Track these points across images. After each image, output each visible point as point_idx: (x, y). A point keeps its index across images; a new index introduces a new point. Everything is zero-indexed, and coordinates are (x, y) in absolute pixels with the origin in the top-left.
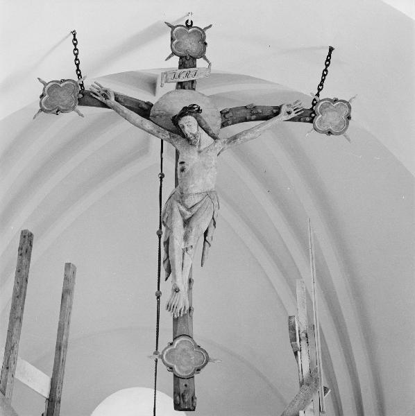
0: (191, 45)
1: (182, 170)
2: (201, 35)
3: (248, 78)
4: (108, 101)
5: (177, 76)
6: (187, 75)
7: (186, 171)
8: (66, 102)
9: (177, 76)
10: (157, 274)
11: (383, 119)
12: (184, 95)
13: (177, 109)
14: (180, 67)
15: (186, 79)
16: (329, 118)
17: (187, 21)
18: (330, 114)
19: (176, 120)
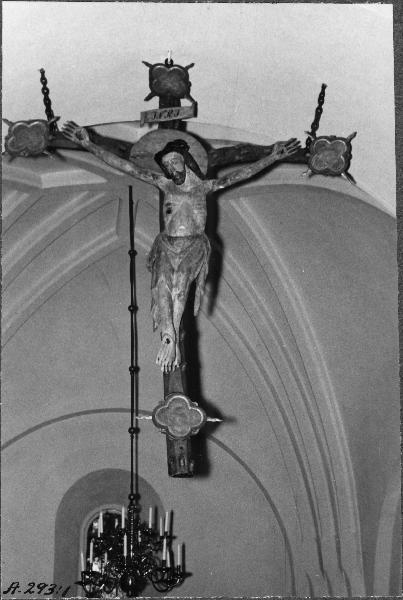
0: (171, 84)
1: (169, 212)
2: (183, 74)
3: (214, 294)
4: (82, 141)
5: (158, 115)
6: (169, 115)
7: (174, 212)
8: (35, 143)
9: (158, 115)
10: (186, 553)
11: (376, 175)
12: (166, 134)
13: (159, 148)
14: (161, 107)
15: (168, 119)
16: (324, 159)
17: (167, 60)
18: (326, 153)
19: (159, 157)
